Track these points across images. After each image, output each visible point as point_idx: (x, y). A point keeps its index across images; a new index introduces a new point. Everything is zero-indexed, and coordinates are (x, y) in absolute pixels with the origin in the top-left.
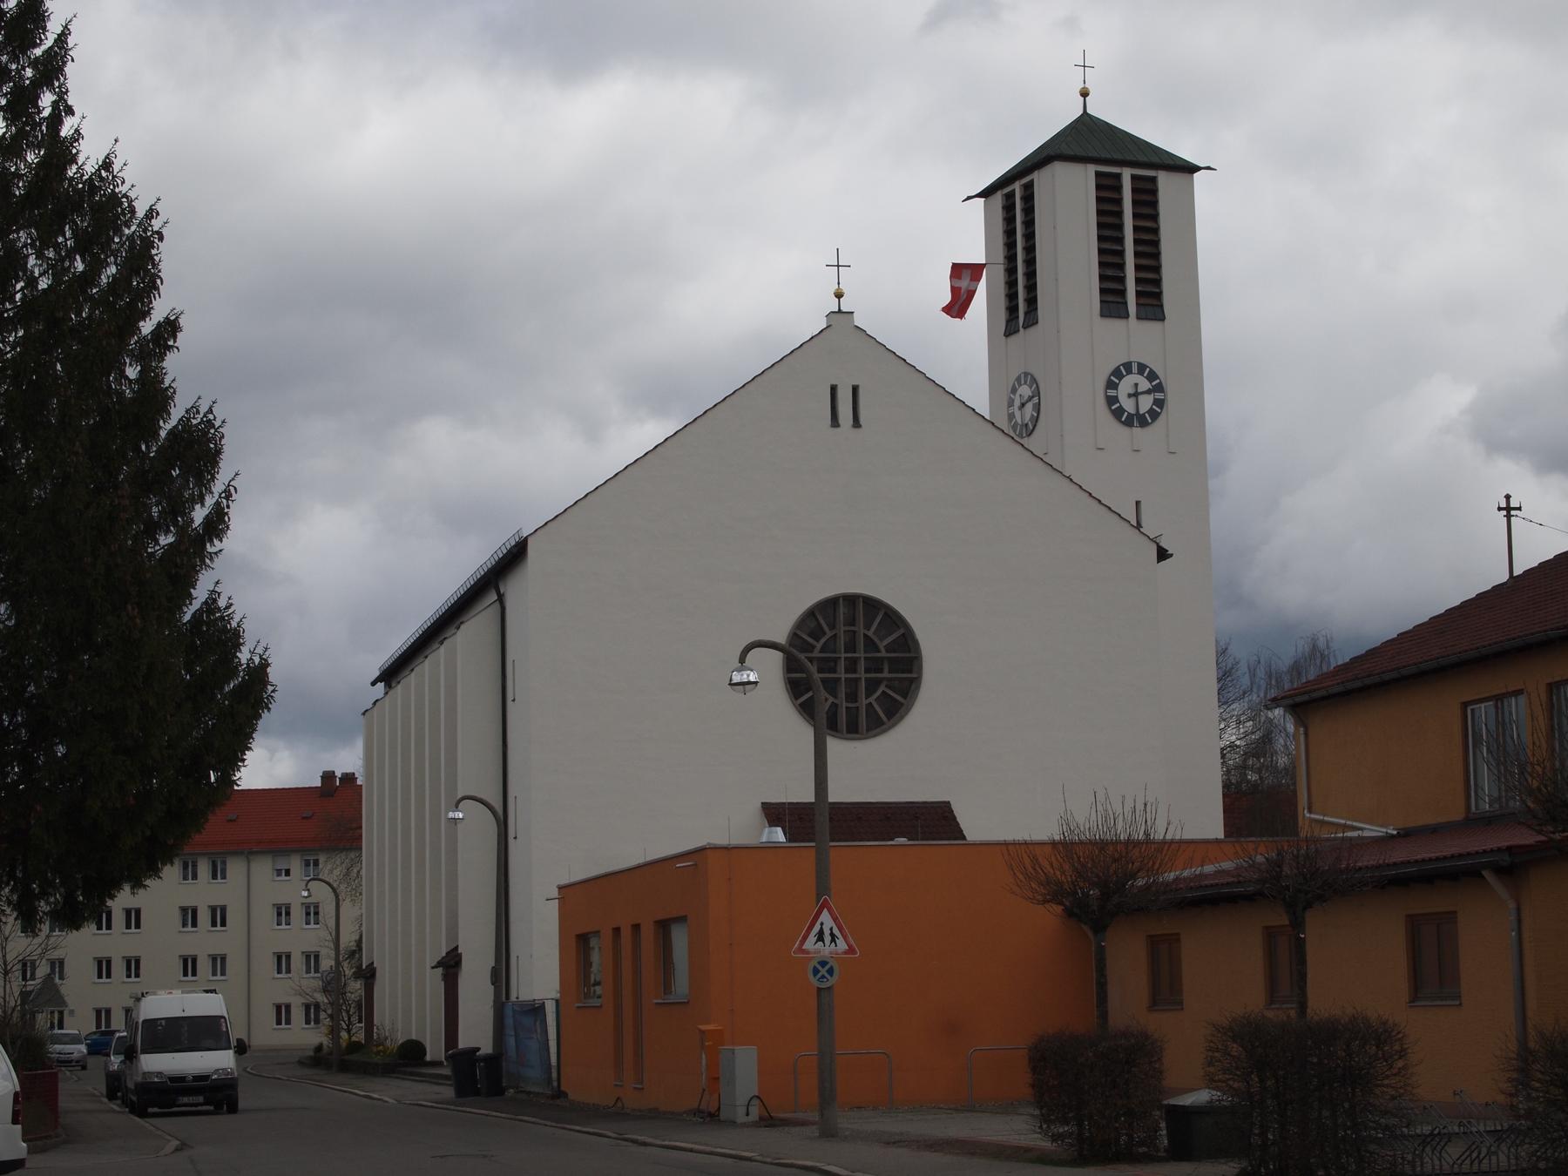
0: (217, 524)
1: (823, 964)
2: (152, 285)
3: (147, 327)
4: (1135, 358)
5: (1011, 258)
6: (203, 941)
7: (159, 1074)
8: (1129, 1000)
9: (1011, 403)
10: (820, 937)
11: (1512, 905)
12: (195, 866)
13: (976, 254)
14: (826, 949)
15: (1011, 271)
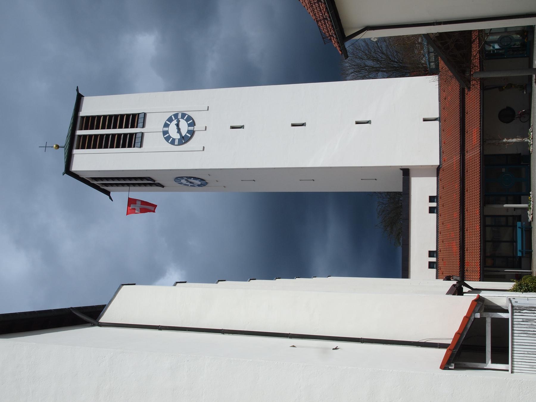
4: (161, 128)
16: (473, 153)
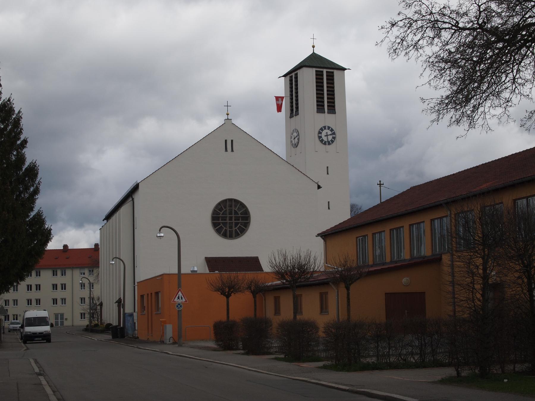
0: (36, 191)
1: (179, 304)
2: (20, 132)
3: (19, 142)
4: (327, 125)
5: (291, 95)
6: (59, 294)
7: (30, 332)
8: (270, 313)
9: (291, 138)
10: (179, 298)
11: (336, 290)
12: (56, 272)
13: (282, 94)
14: (180, 301)
15: (292, 99)
16: (441, 202)
